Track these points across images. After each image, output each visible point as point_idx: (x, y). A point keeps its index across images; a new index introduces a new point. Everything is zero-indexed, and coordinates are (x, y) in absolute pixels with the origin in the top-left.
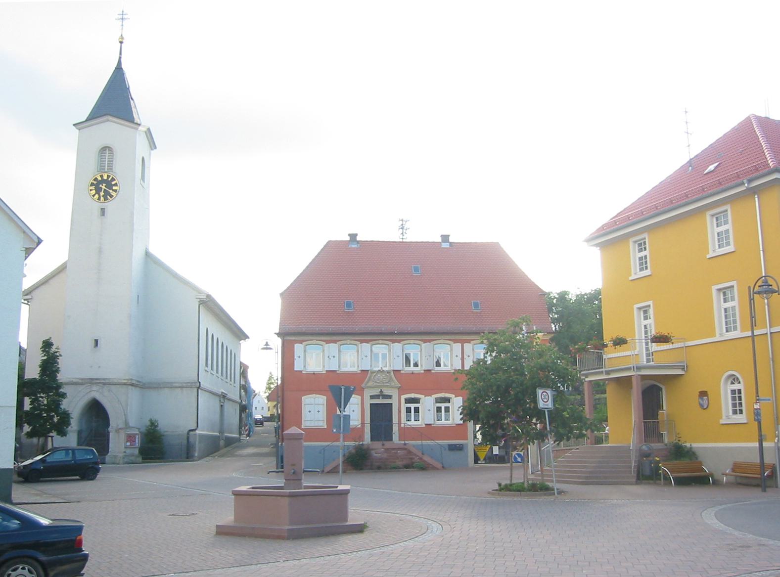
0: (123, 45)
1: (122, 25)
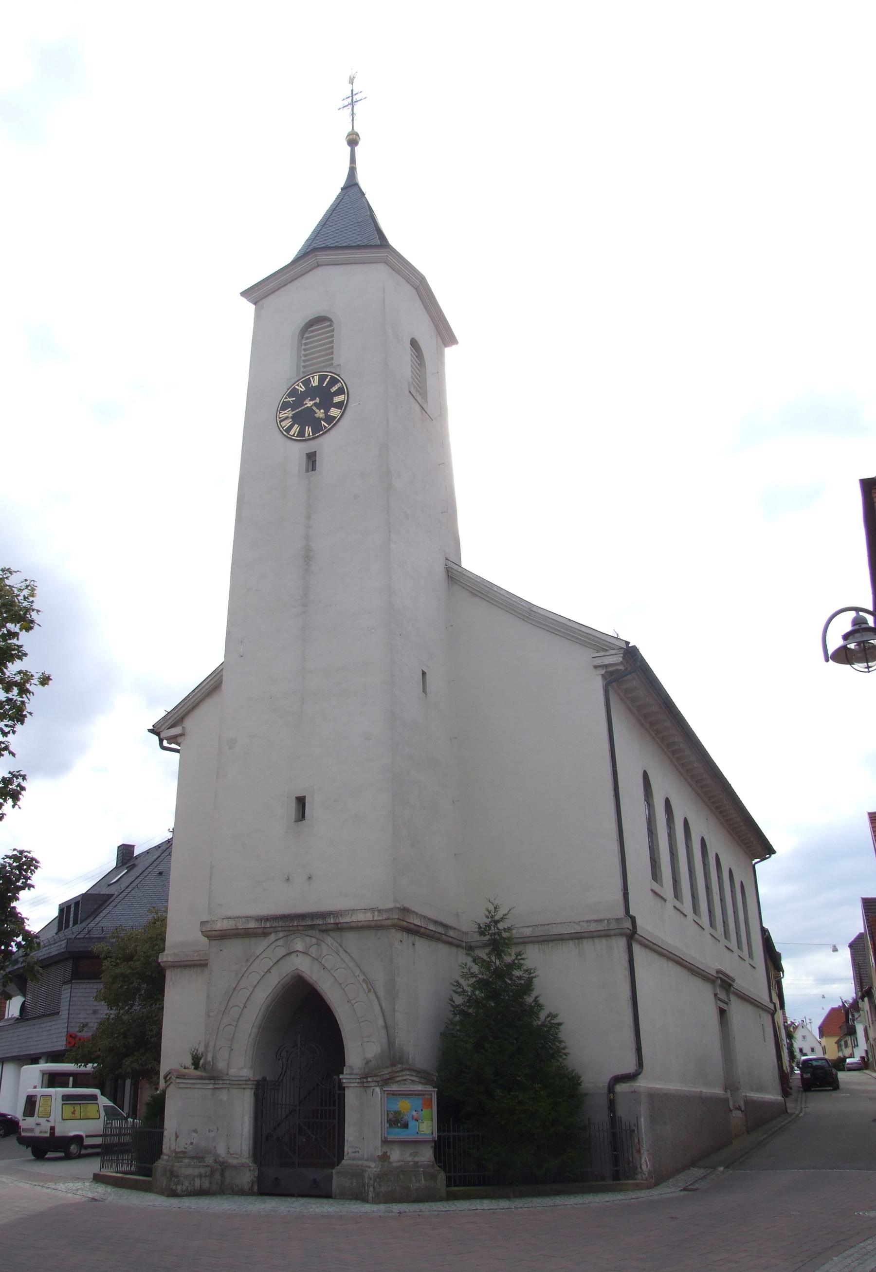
1: (353, 141)
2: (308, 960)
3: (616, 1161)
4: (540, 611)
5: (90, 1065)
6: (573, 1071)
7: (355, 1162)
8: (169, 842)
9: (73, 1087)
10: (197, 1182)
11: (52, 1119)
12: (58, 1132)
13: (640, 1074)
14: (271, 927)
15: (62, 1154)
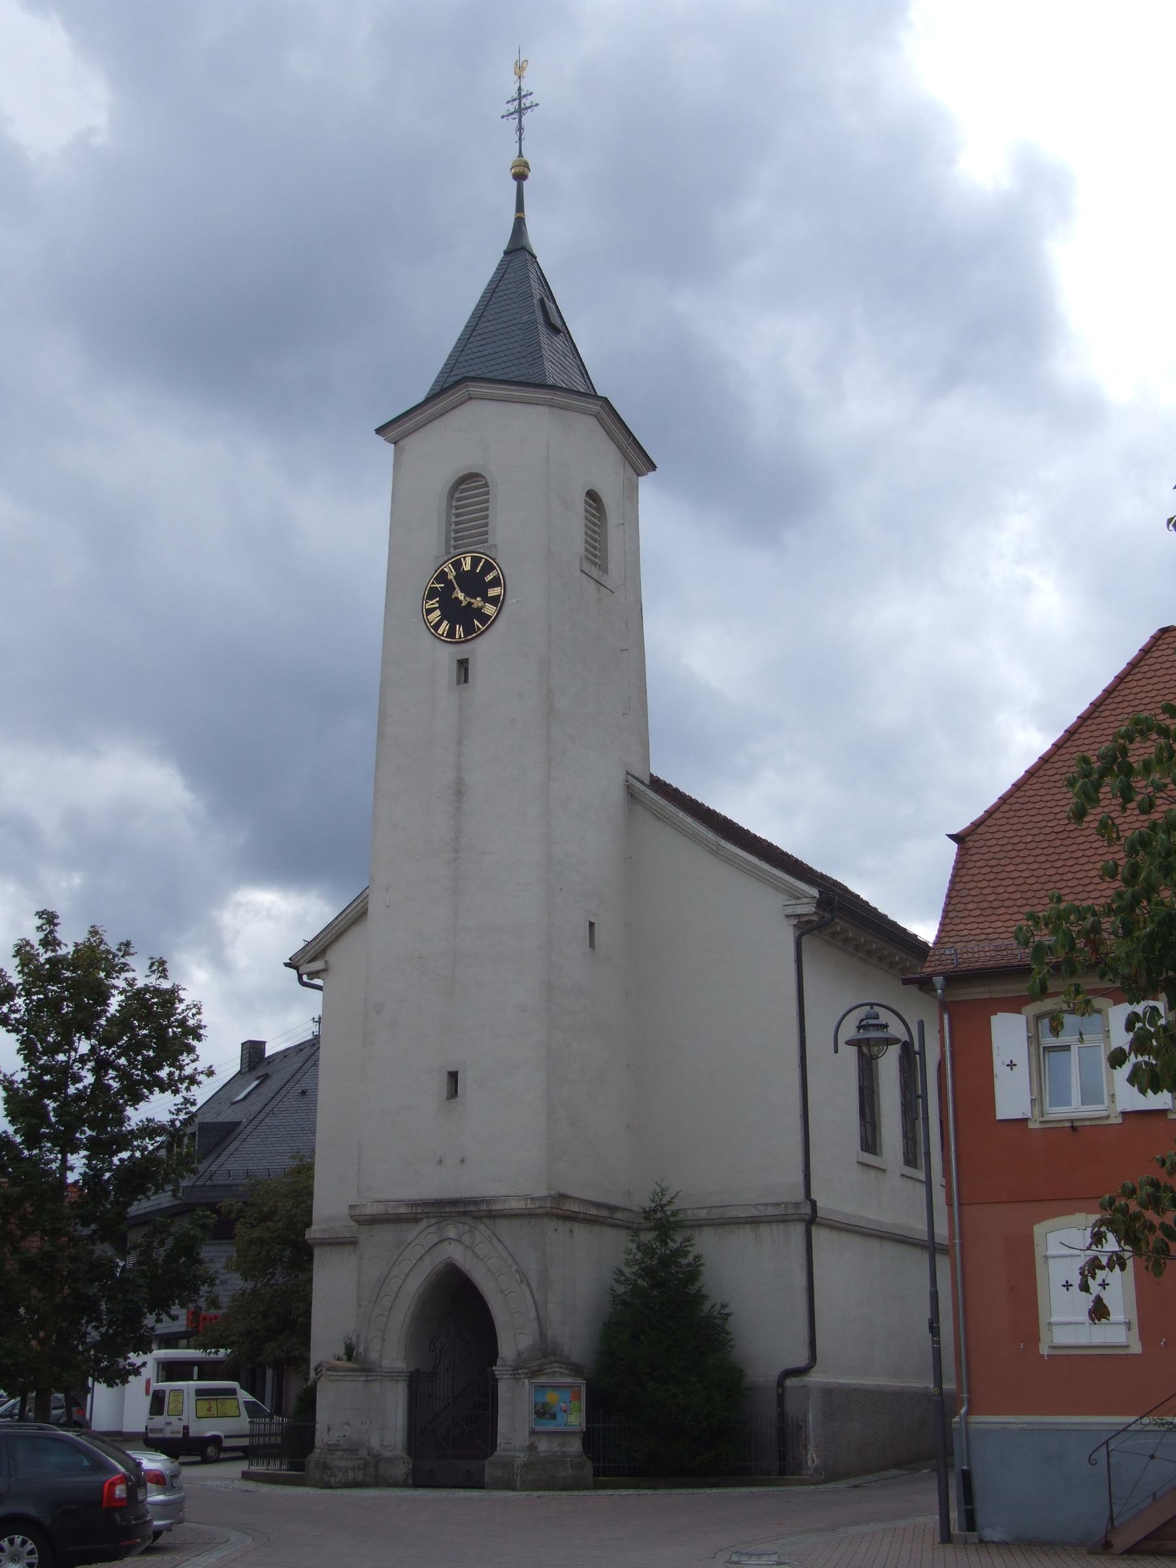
0: (525, 183)
3: (782, 1456)
5: (222, 1351)
8: (314, 1044)
9: (199, 1379)
10: (351, 1475)
11: (184, 1417)
12: (193, 1433)
15: (198, 1458)
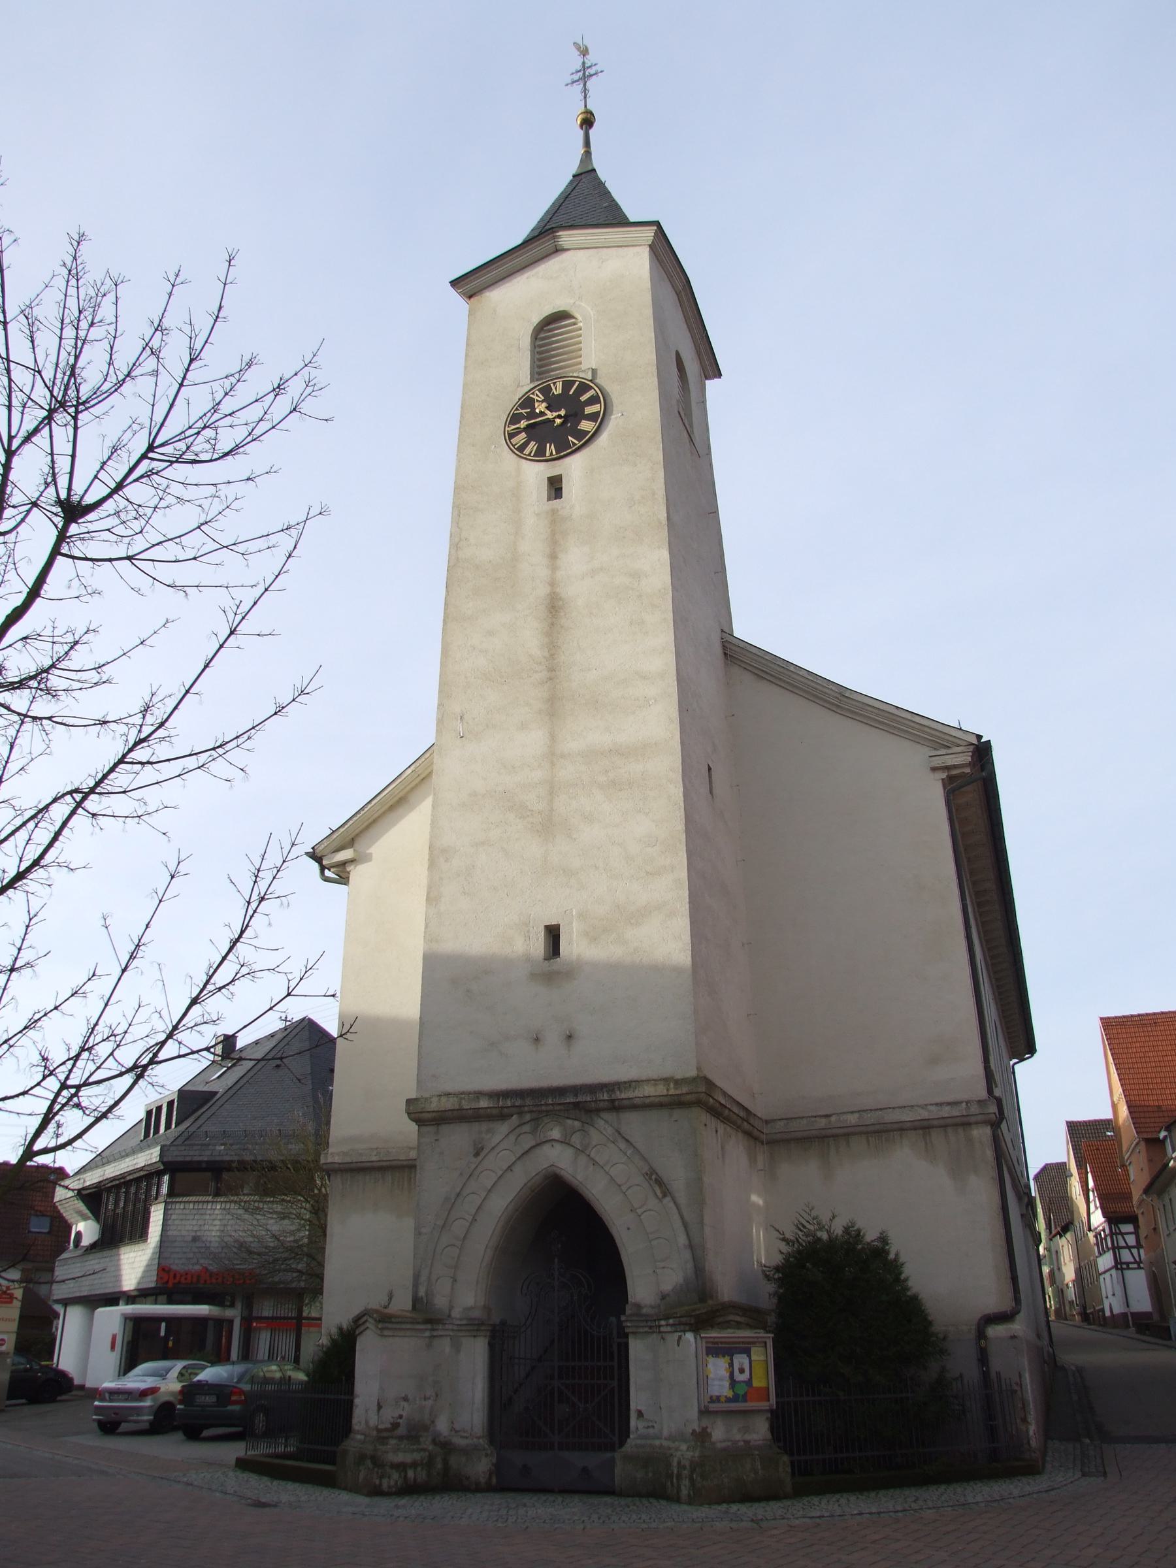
1: (588, 122)
2: (569, 1152)
4: (854, 696)
6: (340, 1329)
7: (649, 1442)
13: (1018, 1312)
14: (513, 1106)
